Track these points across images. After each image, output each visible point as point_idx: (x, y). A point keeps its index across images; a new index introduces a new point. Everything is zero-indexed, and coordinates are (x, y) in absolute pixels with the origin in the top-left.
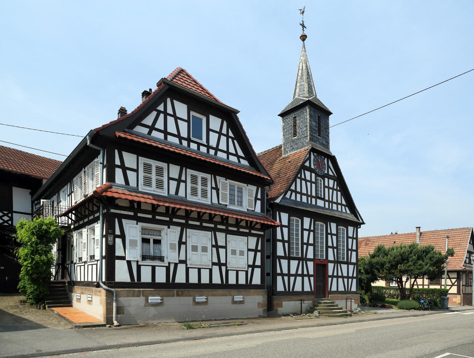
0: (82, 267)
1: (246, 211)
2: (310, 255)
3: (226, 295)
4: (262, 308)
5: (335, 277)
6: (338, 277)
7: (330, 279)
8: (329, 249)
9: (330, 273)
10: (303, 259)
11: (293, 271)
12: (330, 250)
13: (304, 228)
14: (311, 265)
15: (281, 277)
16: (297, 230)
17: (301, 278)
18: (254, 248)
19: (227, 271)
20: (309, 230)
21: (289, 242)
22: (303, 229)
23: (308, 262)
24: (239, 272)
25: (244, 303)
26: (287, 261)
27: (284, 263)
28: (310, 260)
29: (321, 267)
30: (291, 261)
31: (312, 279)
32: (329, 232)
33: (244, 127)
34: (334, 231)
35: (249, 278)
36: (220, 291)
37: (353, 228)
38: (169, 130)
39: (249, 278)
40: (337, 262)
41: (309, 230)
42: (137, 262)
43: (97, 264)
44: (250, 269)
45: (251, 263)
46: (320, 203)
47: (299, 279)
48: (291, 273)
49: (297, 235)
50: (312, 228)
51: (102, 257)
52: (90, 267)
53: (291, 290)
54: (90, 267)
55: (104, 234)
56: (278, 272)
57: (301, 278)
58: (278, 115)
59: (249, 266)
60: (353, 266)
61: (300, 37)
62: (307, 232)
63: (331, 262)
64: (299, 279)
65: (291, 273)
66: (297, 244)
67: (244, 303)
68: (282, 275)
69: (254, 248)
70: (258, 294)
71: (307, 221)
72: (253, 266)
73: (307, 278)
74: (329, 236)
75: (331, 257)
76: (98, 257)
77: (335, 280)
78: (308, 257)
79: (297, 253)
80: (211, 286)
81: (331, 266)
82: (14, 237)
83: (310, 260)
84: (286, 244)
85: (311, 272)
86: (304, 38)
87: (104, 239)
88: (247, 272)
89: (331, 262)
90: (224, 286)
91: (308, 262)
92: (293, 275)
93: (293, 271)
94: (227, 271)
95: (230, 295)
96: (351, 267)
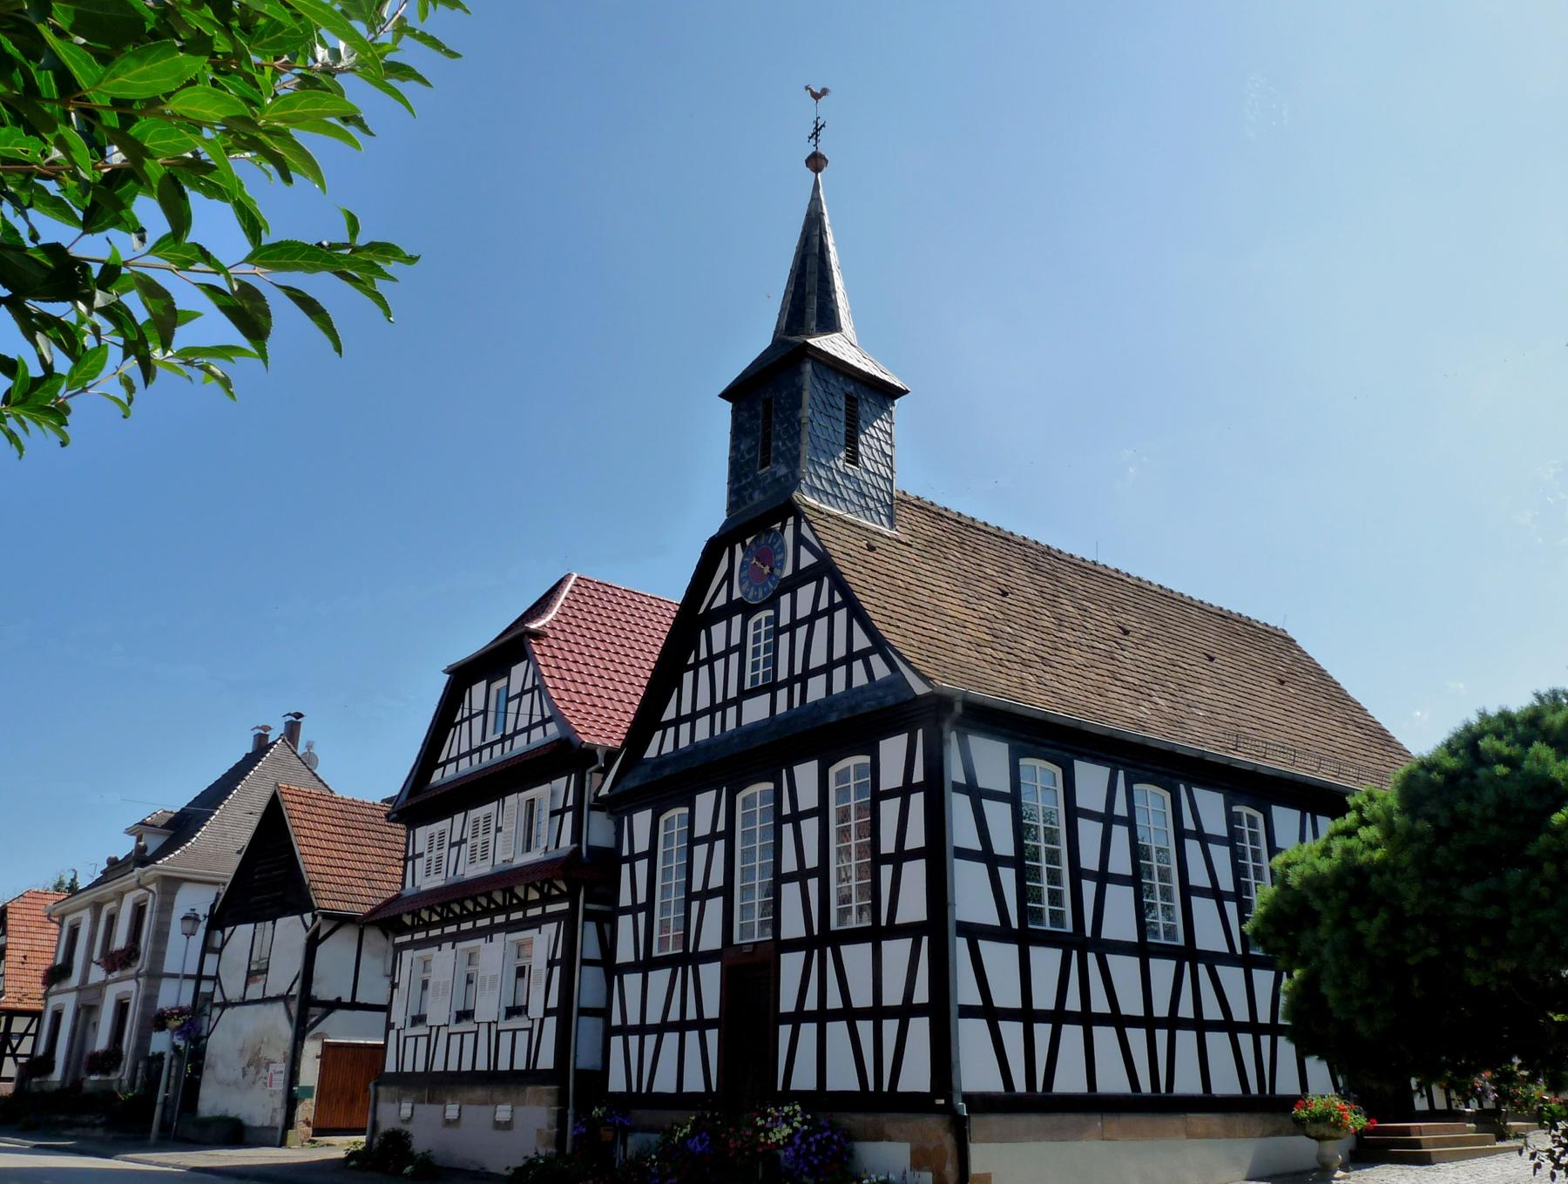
0: (469, 1039)
2: (1120, 922)
5: (1073, 1018)
6: (1087, 1019)
7: (785, 1031)
8: (1196, 901)
9: (787, 1004)
10: (1082, 943)
11: (1044, 999)
15: (1156, 1014)
17: (886, 1002)
20: (1103, 877)
24: (384, 1014)
26: (1012, 950)
27: (1000, 958)
28: (709, 957)
31: (712, 1036)
33: (794, 251)
34: (1204, 908)
36: (1197, 1120)
37: (1297, 813)
38: (746, 704)
41: (1103, 877)
43: (476, 1033)
46: (520, 743)
47: (1072, 1035)
51: (548, 1012)
52: (455, 1040)
53: (644, 1090)
54: (455, 1040)
55: (558, 956)
63: (793, 945)
64: (893, 996)
68: (990, 1013)
76: (536, 1010)
77: (808, 1031)
79: (1057, 917)
81: (791, 964)
83: (709, 957)
84: (1008, 876)
85: (712, 1010)
87: (557, 970)
89: (793, 945)
93: (1044, 999)
96: (804, 1079)
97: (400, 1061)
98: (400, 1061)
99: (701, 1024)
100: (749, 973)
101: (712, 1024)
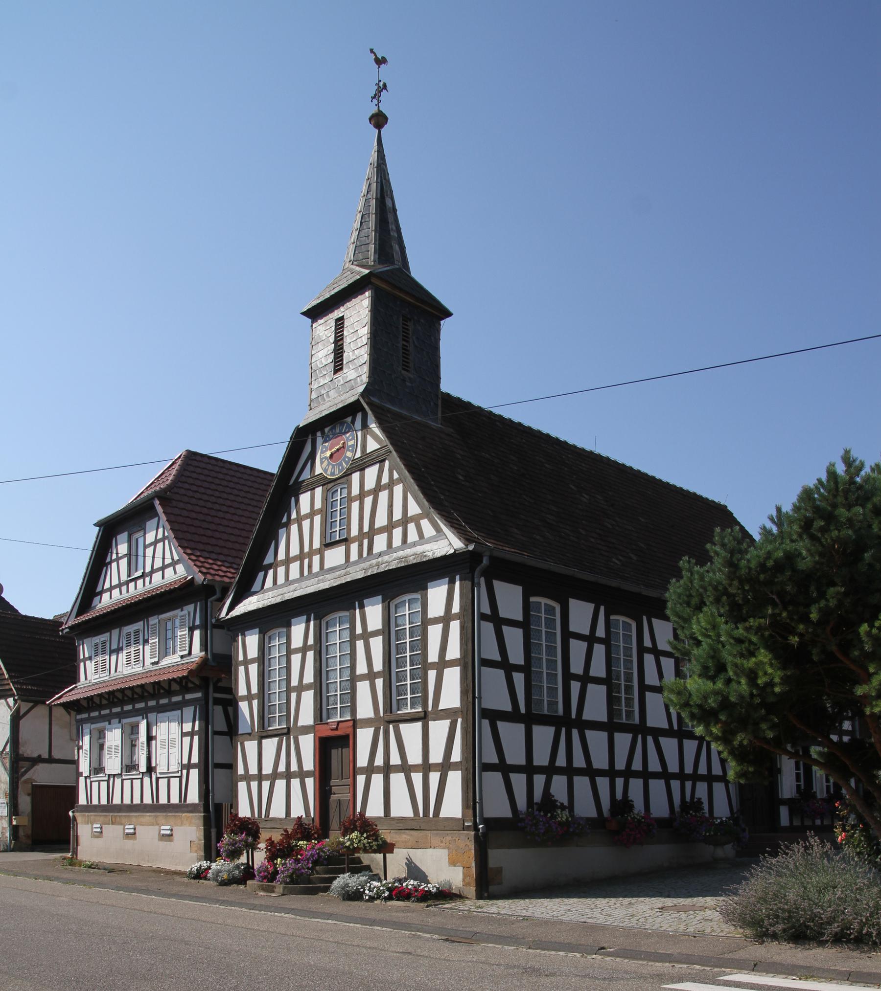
1: (179, 659)
3: (152, 825)
4: (196, 852)
6: (288, 775)
9: (362, 761)
11: (541, 758)
12: (363, 688)
13: (572, 628)
14: (307, 743)
16: (551, 636)
17: (640, 781)
18: (591, 687)
19: (157, 779)
21: (526, 668)
22: (567, 636)
23: (589, 733)
24: (172, 779)
25: (171, 841)
26: (521, 728)
28: (306, 730)
29: (334, 745)
30: (617, 735)
32: (647, 643)
35: (183, 793)
39: (183, 793)
40: (390, 718)
42: (120, 775)
44: (185, 772)
45: (185, 761)
48: (537, 762)
49: (551, 650)
50: (601, 632)
56: (239, 773)
57: (640, 781)
58: (304, 314)
59: (183, 767)
60: (629, 736)
61: (370, 119)
62: (584, 645)
63: (596, 726)
65: (537, 762)
66: (552, 677)
67: (135, 839)
69: (591, 687)
70: (190, 824)
71: (581, 613)
72: (189, 766)
73: (586, 779)
74: (649, 659)
75: (365, 709)
78: (586, 716)
80: (141, 808)
81: (364, 737)
82: (353, 422)
84: (519, 678)
86: (379, 120)
88: (181, 777)
90: (156, 808)
91: (589, 733)
92: (540, 770)
93: (541, 758)
94: (157, 779)
95: (158, 824)
97: (89, 798)
98: (89, 798)
99: (302, 775)
100: (334, 745)
101: (309, 774)
